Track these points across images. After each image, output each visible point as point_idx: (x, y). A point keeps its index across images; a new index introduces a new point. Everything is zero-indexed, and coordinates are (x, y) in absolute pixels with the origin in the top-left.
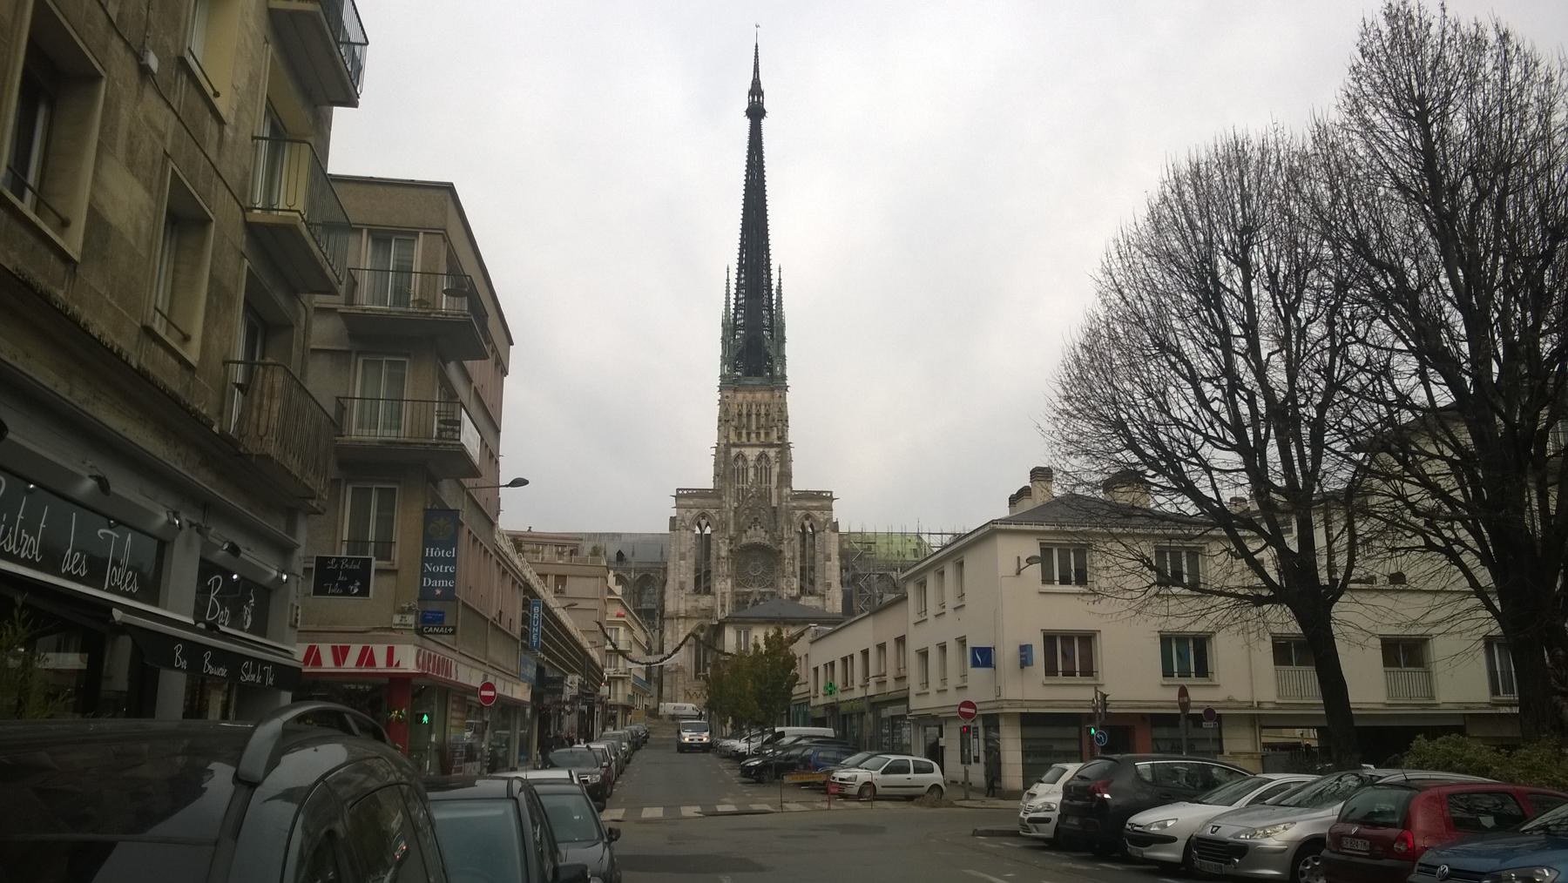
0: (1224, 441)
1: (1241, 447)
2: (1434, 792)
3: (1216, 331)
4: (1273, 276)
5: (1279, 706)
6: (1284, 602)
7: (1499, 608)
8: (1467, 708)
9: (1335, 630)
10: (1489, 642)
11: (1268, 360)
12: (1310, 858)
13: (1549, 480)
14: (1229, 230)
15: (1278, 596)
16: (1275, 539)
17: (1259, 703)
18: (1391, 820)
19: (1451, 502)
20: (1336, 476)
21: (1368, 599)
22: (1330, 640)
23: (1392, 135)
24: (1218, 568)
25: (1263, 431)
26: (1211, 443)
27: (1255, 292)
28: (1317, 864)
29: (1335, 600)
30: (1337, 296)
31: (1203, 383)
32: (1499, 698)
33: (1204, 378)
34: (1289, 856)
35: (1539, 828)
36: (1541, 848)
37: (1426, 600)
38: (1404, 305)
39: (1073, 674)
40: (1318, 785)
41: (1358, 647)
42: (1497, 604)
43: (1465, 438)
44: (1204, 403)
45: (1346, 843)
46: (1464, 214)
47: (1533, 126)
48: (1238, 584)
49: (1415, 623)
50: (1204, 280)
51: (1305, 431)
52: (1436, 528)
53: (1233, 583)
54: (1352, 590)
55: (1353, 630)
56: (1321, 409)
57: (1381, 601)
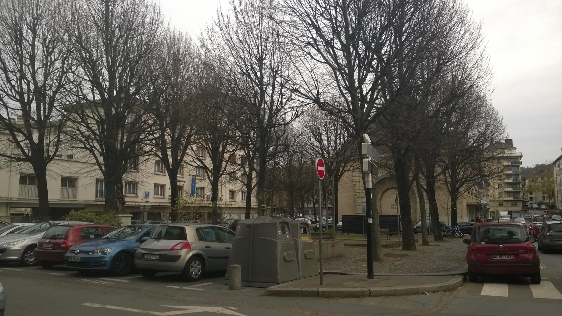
0: (15, 97)
1: (21, 101)
2: (77, 227)
3: (18, 53)
4: (45, 40)
5: (19, 199)
6: (28, 161)
7: (104, 170)
8: (87, 202)
9: (47, 173)
10: (98, 181)
11: (37, 70)
12: (29, 252)
13: (125, 131)
14: (30, 17)
15: (27, 159)
16: (29, 137)
17: (11, 198)
18: (61, 237)
19: (94, 134)
20: (56, 117)
21: (59, 162)
22: (45, 176)
23: (96, 5)
24: (3, 146)
25: (31, 97)
26: (9, 97)
27: (36, 43)
28: (32, 253)
29: (49, 162)
30: (67, 53)
31: (9, 73)
32: (97, 199)
33: (10, 71)
34: (22, 251)
35: (105, 238)
36: (106, 243)
37: (80, 165)
38: (90, 65)
39: (130, 193)
40: (35, 227)
41: (54, 180)
42: (103, 168)
43: (103, 114)
44: (9, 80)
45: (45, 245)
46: (115, 40)
47: (140, 19)
48: (11, 152)
49: (76, 173)
50: (16, 32)
51: (47, 100)
52: (89, 142)
53: (9, 152)
54: (55, 159)
55: (53, 173)
56: (55, 93)
57: (66, 164)
